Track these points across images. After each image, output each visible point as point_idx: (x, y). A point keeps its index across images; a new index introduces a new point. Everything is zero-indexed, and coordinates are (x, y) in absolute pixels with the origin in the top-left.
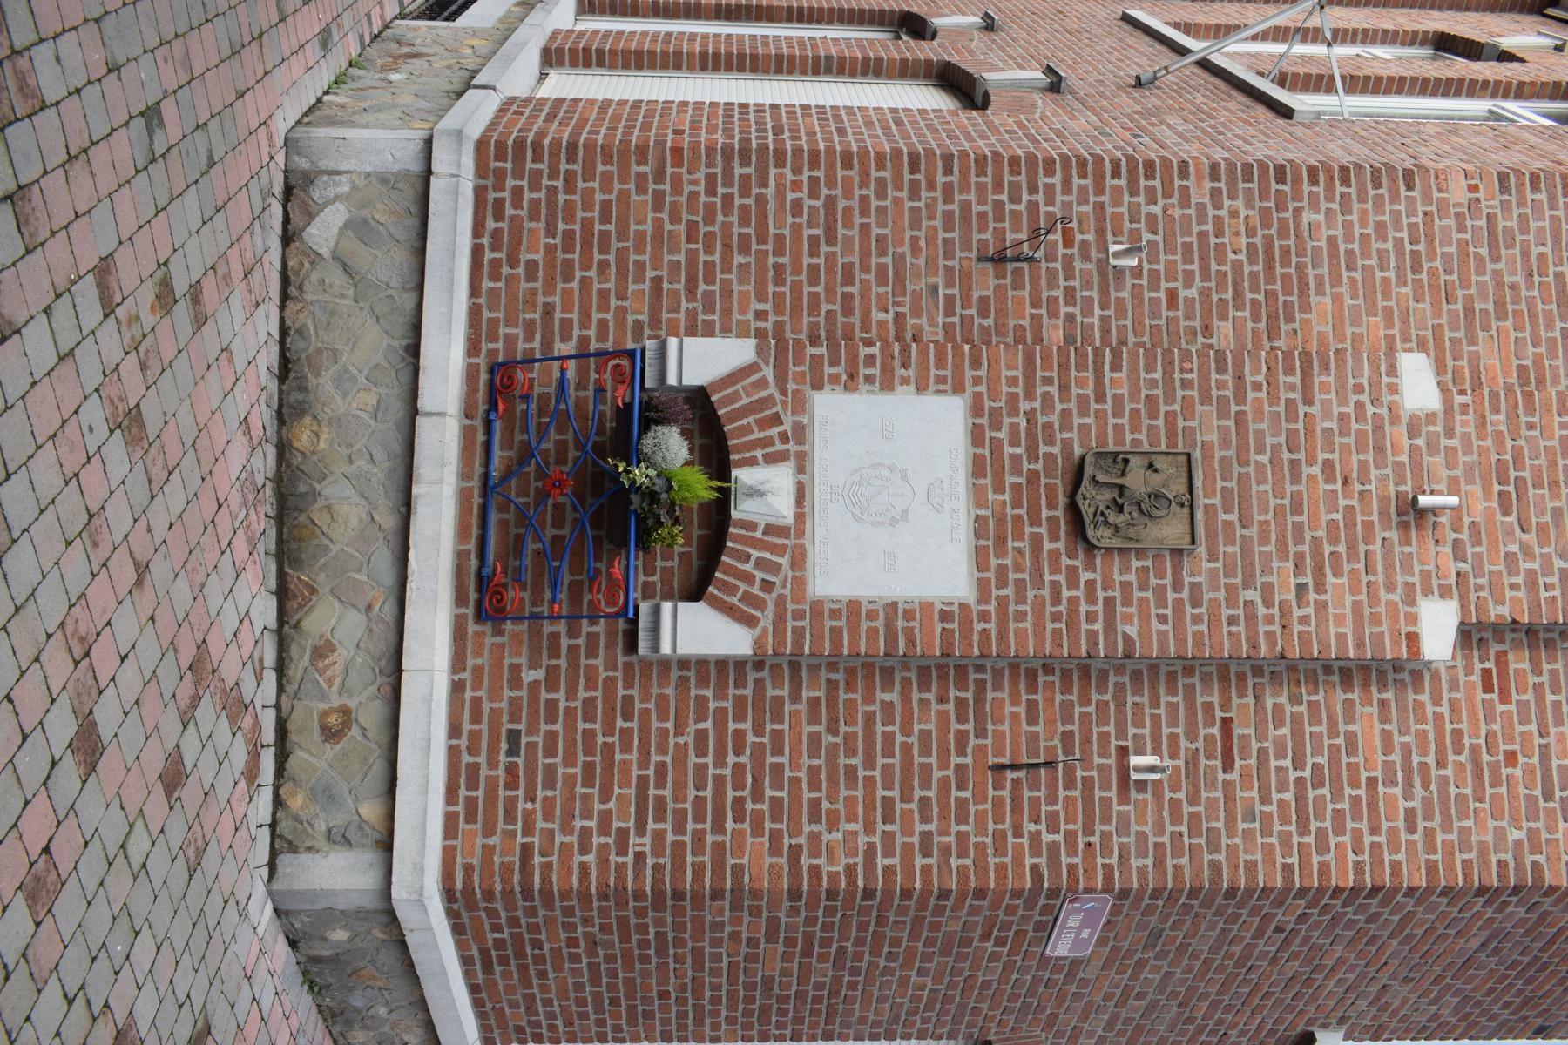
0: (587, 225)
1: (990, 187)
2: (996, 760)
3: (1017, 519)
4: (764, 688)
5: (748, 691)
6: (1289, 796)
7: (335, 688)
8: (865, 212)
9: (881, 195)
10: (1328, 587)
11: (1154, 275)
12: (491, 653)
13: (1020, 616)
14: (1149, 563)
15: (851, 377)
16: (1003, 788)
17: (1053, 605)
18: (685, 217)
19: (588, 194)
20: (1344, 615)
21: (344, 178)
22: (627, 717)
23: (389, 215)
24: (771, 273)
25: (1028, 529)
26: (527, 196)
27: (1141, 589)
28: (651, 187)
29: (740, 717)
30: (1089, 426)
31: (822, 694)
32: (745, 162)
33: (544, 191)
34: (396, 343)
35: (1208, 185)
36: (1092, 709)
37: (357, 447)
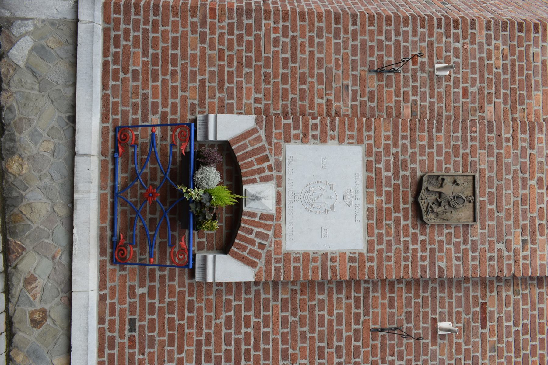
0: (165, 50)
1: (376, 32)
2: (374, 327)
3: (388, 209)
4: (260, 294)
5: (252, 296)
6: (511, 339)
7: (37, 299)
8: (311, 45)
9: (320, 36)
10: (537, 241)
11: (457, 80)
12: (119, 280)
13: (389, 259)
14: (452, 231)
15: (305, 135)
16: (377, 340)
17: (405, 253)
18: (217, 46)
19: (165, 33)
20: (544, 255)
21: (30, 22)
22: (190, 311)
23: (56, 44)
24: (263, 78)
25: (393, 215)
26: (132, 34)
27: (448, 244)
28: (199, 30)
29: (248, 309)
30: (425, 161)
31: (289, 296)
32: (249, 17)
33: (141, 31)
34: (63, 115)
35: (485, 32)
36: (420, 300)
37: (44, 171)
